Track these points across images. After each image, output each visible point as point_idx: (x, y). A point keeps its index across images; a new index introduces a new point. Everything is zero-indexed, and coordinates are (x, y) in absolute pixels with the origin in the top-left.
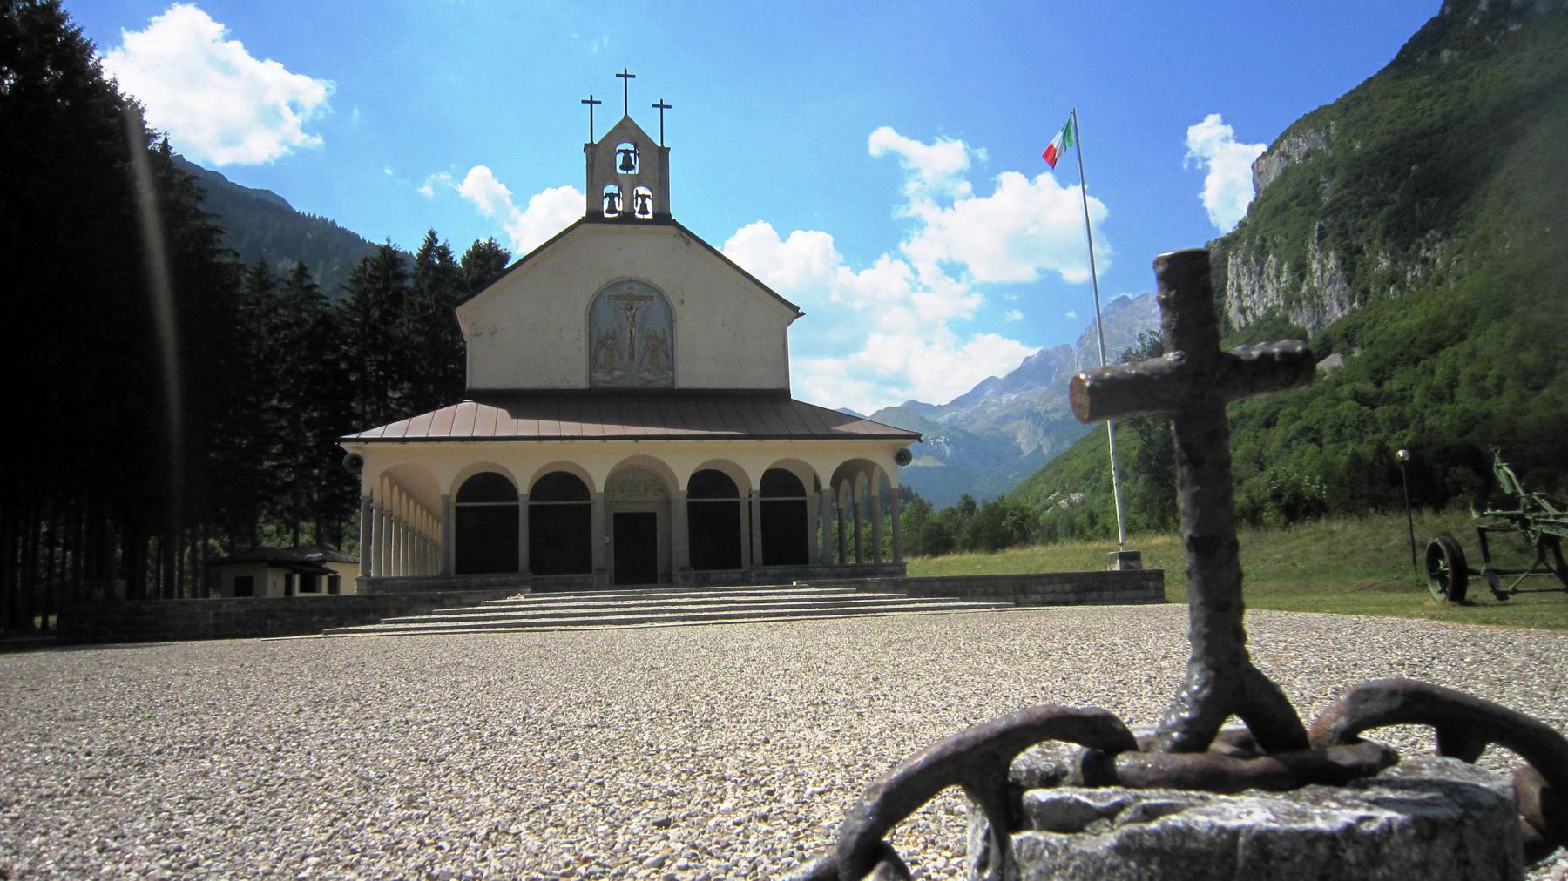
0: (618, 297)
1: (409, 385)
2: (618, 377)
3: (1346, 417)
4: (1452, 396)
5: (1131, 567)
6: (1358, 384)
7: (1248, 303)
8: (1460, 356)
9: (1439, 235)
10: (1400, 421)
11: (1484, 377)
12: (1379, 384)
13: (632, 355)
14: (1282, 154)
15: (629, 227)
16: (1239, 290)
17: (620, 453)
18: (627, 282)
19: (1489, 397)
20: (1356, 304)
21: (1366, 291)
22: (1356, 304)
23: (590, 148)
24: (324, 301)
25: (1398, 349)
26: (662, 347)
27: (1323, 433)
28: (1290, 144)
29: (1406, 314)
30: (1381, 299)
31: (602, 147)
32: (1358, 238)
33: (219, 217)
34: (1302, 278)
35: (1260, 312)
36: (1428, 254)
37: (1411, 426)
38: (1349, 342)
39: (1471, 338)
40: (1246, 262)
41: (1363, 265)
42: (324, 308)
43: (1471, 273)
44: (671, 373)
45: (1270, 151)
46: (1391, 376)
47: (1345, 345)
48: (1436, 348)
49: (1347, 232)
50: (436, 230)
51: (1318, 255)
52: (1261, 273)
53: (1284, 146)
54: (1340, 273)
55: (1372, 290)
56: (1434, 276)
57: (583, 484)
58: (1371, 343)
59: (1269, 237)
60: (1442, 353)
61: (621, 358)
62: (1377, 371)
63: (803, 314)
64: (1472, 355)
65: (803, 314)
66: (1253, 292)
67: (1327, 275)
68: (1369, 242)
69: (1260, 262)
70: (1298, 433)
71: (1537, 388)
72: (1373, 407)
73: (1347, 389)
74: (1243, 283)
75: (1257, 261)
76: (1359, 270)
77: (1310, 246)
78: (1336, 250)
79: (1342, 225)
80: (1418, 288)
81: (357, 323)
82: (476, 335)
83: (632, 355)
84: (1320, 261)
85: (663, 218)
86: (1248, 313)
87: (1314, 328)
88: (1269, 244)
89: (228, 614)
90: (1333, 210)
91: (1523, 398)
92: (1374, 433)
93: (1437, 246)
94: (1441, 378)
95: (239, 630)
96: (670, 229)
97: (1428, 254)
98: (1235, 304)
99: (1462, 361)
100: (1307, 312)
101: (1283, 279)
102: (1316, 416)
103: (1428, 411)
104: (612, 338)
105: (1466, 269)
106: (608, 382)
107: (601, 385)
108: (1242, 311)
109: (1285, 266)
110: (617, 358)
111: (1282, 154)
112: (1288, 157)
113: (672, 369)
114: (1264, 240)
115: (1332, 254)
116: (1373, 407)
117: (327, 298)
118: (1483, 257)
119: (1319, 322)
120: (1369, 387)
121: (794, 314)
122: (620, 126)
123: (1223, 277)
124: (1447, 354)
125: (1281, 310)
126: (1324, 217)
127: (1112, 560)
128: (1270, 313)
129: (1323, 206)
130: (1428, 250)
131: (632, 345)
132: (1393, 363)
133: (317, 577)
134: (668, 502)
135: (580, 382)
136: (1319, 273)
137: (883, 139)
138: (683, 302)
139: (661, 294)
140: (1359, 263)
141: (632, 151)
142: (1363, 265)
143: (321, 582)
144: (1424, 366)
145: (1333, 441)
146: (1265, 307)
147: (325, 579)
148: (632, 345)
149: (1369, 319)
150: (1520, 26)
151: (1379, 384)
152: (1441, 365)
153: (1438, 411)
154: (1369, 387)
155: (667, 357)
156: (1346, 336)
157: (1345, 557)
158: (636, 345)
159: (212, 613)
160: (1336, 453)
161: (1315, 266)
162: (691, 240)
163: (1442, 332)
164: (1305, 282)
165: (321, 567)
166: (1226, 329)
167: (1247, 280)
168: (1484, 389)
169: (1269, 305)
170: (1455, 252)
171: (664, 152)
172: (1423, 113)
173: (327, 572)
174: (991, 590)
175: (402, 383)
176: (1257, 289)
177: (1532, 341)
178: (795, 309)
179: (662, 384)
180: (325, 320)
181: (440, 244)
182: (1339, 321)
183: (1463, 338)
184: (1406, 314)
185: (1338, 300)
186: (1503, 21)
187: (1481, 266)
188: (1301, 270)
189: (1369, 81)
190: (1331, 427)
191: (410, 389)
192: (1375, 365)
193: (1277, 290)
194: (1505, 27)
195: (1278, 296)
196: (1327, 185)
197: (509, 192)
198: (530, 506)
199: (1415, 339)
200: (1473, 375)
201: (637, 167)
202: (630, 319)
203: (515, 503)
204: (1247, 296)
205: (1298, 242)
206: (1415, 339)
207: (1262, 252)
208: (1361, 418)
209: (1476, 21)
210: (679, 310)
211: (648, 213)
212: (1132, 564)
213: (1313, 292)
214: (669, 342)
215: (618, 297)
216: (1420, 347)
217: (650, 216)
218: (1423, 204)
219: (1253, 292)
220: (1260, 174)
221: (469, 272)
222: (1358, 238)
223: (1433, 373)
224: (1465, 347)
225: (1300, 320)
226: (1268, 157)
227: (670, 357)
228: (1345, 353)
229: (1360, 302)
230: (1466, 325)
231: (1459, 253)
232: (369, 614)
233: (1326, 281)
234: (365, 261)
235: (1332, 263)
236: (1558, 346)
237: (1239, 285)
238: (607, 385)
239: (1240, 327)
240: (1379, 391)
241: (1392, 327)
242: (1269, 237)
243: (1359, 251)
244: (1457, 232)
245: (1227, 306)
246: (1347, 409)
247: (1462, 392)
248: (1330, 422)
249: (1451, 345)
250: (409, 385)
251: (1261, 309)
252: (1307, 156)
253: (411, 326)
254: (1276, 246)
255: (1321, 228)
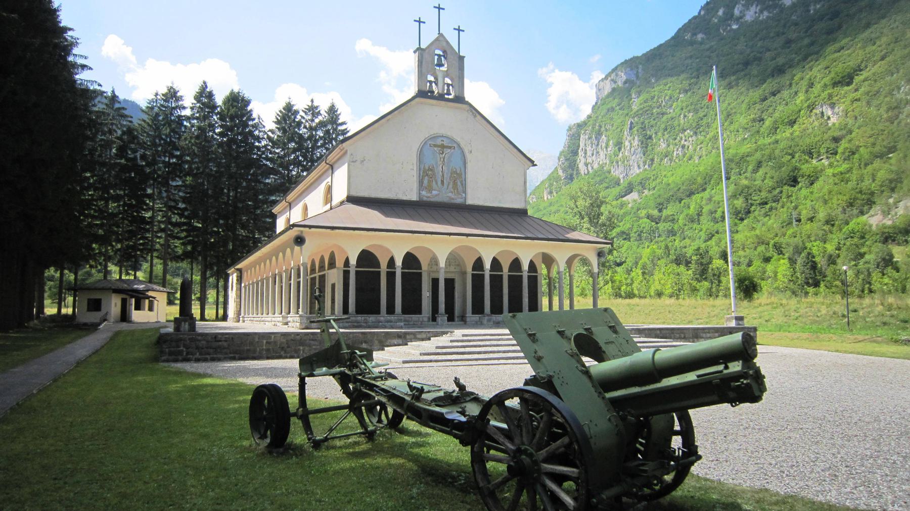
0: (435, 146)
1: (191, 179)
2: (441, 194)
3: (644, 228)
4: (699, 220)
5: (739, 325)
6: (650, 210)
7: (589, 160)
8: (704, 199)
9: (692, 133)
10: (672, 232)
11: (716, 211)
12: (660, 211)
13: (442, 182)
14: (612, 80)
15: (443, 103)
16: (586, 153)
17: (453, 244)
18: (440, 136)
19: (717, 222)
20: (647, 166)
21: (652, 160)
22: (647, 166)
23: (419, 50)
24: (130, 119)
25: (671, 193)
26: (459, 179)
27: (631, 235)
28: (617, 75)
29: (673, 175)
30: (660, 165)
31: (427, 51)
32: (650, 131)
33: (86, 58)
34: (620, 149)
35: (596, 166)
36: (685, 143)
37: (678, 235)
38: (643, 187)
39: (708, 190)
40: (590, 138)
41: (652, 146)
42: (128, 123)
43: (707, 155)
44: (464, 195)
45: (606, 78)
46: (667, 207)
47: (640, 188)
48: (691, 194)
49: (645, 127)
50: (207, 81)
51: (628, 138)
52: (598, 145)
53: (613, 76)
54: (640, 149)
55: (656, 159)
56: (688, 155)
57: (416, 257)
58: (654, 189)
59: (603, 126)
60: (694, 197)
61: (437, 183)
62: (660, 204)
63: (536, 165)
64: (710, 199)
65: (536, 165)
66: (593, 155)
67: (633, 149)
68: (656, 133)
69: (598, 138)
70: (618, 234)
71: (742, 219)
72: (657, 223)
73: (643, 213)
74: (588, 149)
75: (596, 138)
76: (650, 148)
77: (625, 133)
78: (639, 136)
79: (643, 123)
80: (679, 160)
81: (151, 135)
82: (353, 162)
83: (442, 182)
84: (630, 141)
85: (460, 99)
86: (589, 166)
87: (624, 178)
88: (603, 129)
89: (275, 342)
90: (636, 115)
91: (736, 225)
92: (658, 237)
93: (690, 139)
94: (694, 211)
95: (282, 353)
96: (464, 106)
97: (685, 143)
98: (583, 160)
99: (704, 202)
100: (621, 169)
101: (609, 149)
102: (628, 226)
103: (686, 228)
104: (431, 170)
105: (704, 153)
106: (429, 197)
107: (425, 199)
108: (586, 165)
109: (611, 142)
110: (434, 183)
111: (612, 80)
112: (615, 82)
113: (465, 192)
114: (600, 126)
115: (636, 138)
116: (657, 223)
117: (132, 117)
118: (713, 148)
119: (626, 175)
120: (655, 213)
121: (531, 164)
122: (437, 40)
123: (577, 145)
124: (697, 197)
125: (607, 166)
126: (633, 118)
127: (729, 320)
128: (602, 167)
129: (633, 112)
130: (686, 141)
131: (443, 176)
132: (668, 201)
133: (142, 300)
134: (463, 273)
135: (414, 197)
136: (629, 148)
137: (363, 45)
138: (471, 152)
139: (459, 145)
140: (650, 145)
141: (442, 56)
142: (652, 146)
143: (144, 302)
144: (685, 203)
145: (636, 240)
146: (599, 164)
147: (147, 301)
148: (443, 176)
149: (654, 175)
150: (737, 27)
151: (660, 211)
152: (694, 203)
153: (692, 228)
154: (655, 213)
155: (462, 185)
156: (641, 183)
157: (797, 319)
158: (445, 176)
159: (265, 341)
160: (638, 247)
161: (627, 143)
162: (477, 115)
163: (694, 186)
164: (621, 152)
165: (145, 294)
166: (577, 174)
167: (590, 147)
168: (715, 218)
169: (601, 163)
170: (699, 143)
171: (461, 59)
172: (687, 67)
173: (148, 297)
174: (682, 336)
175: (186, 177)
176: (595, 153)
177: (740, 195)
178: (532, 162)
179: (459, 201)
180: (130, 131)
181: (208, 90)
182: (638, 175)
183: (704, 190)
184: (673, 175)
185: (637, 163)
186: (729, 22)
187: (712, 151)
188: (619, 145)
189: (661, 46)
190: (636, 232)
191: (192, 181)
192: (659, 200)
193: (606, 155)
194: (730, 25)
195: (606, 158)
196: (635, 100)
197: (130, 49)
198: (387, 272)
199: (680, 188)
200: (710, 210)
201: (446, 66)
202: (442, 159)
203: (379, 270)
204: (589, 156)
205: (619, 130)
206: (680, 188)
207: (599, 134)
208: (652, 229)
209: (716, 21)
210: (469, 156)
211: (450, 94)
212: (740, 323)
213: (625, 159)
214: (463, 176)
215: (435, 146)
216: (683, 193)
217: (450, 97)
218: (685, 116)
219: (593, 155)
220: (599, 90)
221: (229, 110)
222: (650, 131)
223: (689, 207)
224: (706, 195)
225: (617, 172)
226: (605, 81)
227: (464, 185)
228: (640, 193)
229: (649, 166)
230: (706, 184)
231: (701, 144)
232: (362, 344)
233: (632, 153)
234: (157, 94)
235: (636, 142)
236: (753, 198)
237: (586, 150)
238: (428, 200)
239: (585, 174)
240: (660, 214)
241: (665, 180)
242: (603, 126)
243: (650, 137)
244: (701, 132)
245: (578, 161)
246: (645, 223)
247: (704, 219)
248: (635, 230)
249: (698, 193)
250: (191, 179)
251: (597, 164)
252: (625, 83)
253: (193, 141)
254: (606, 130)
255: (632, 123)
